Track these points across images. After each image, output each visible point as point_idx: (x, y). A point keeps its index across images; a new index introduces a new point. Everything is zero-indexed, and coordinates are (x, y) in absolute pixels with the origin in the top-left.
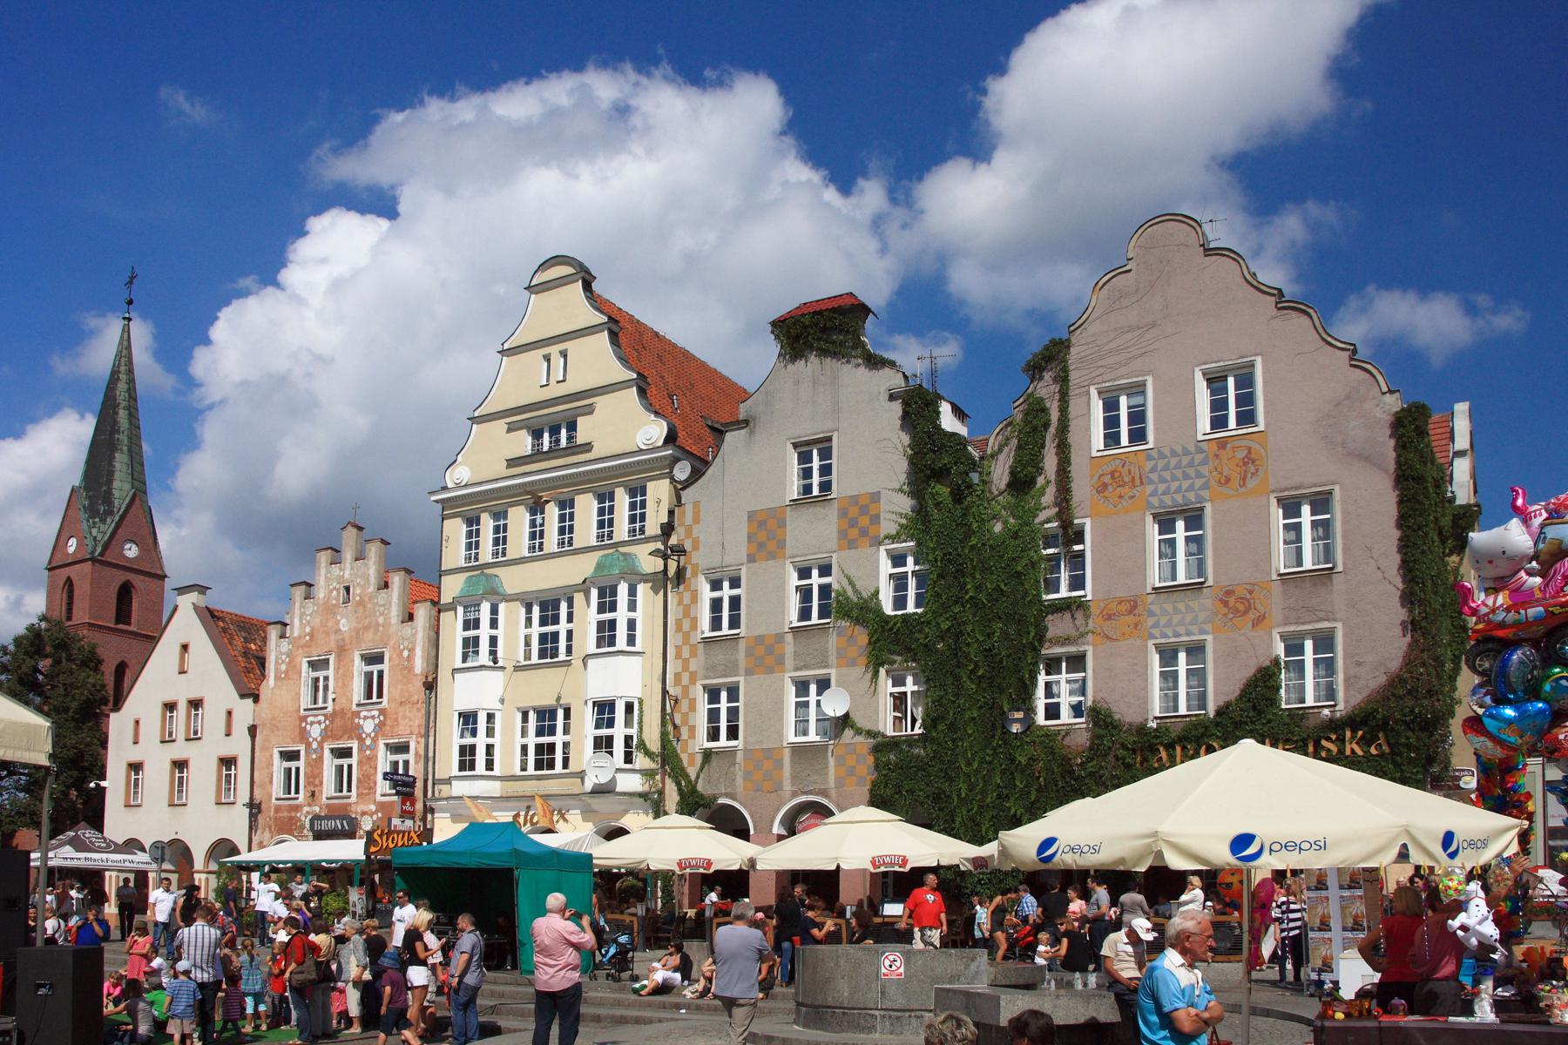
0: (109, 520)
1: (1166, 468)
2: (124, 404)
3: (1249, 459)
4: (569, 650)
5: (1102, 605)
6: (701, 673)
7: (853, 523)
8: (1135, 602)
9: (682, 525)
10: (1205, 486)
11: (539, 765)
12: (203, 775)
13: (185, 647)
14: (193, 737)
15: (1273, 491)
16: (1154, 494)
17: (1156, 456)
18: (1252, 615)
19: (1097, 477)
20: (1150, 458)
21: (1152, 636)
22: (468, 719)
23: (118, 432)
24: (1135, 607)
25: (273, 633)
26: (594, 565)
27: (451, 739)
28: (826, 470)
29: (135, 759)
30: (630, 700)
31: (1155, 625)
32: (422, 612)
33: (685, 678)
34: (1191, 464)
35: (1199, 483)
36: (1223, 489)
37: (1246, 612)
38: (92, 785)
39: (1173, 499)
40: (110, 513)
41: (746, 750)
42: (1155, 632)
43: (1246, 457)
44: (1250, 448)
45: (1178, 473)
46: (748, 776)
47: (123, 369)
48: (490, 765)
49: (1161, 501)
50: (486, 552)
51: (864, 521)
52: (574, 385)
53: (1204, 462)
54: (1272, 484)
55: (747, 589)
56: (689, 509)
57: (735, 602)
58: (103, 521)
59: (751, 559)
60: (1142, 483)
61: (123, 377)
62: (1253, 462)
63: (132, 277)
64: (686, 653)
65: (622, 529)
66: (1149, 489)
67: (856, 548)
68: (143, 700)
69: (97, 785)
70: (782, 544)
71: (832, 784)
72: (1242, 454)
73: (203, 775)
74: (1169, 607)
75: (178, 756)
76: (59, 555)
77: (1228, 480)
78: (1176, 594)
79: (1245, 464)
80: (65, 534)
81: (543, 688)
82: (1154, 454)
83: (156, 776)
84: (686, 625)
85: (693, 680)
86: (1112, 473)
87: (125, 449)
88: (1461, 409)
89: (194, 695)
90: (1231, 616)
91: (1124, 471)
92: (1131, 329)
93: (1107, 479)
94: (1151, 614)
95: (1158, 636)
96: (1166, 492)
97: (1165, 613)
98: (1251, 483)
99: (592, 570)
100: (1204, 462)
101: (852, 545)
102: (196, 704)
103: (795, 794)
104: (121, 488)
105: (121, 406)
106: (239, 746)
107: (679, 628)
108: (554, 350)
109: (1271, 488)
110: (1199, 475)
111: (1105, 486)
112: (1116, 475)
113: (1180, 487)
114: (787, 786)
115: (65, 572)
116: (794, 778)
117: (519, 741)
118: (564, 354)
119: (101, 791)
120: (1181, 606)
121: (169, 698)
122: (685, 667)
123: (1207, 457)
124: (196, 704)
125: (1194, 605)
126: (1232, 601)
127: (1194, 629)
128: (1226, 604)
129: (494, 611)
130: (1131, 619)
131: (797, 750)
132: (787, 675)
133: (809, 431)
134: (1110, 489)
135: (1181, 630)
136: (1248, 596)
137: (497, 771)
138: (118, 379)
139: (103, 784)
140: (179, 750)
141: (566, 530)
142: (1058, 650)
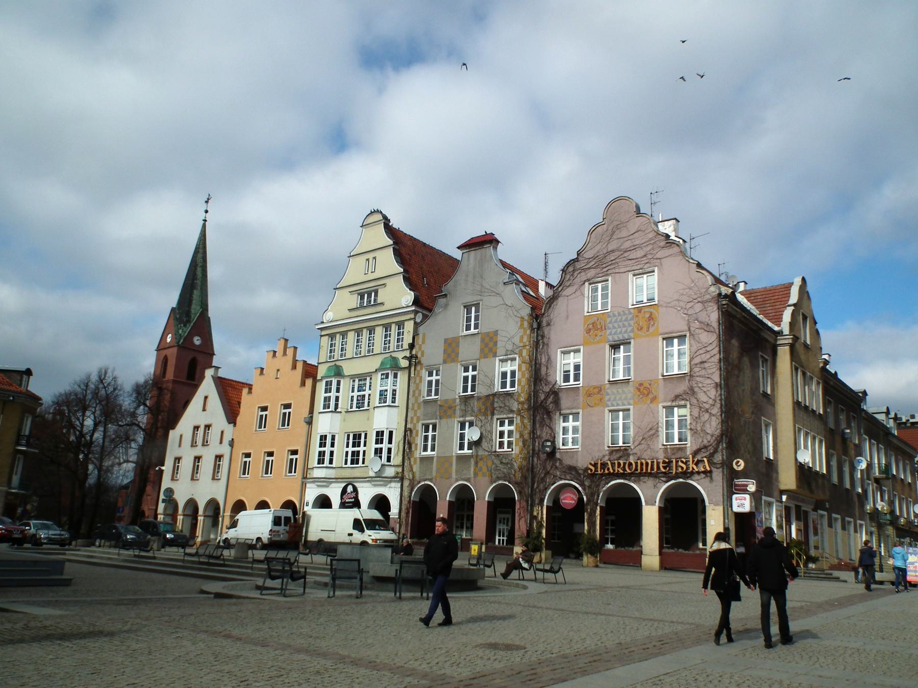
0: (188, 326)
1: (616, 322)
2: (200, 264)
3: (651, 318)
4: (369, 405)
5: (587, 389)
6: (422, 417)
7: (486, 345)
8: (601, 388)
9: (418, 344)
10: (632, 331)
11: (352, 463)
12: (207, 466)
13: (206, 398)
14: (205, 443)
15: (661, 334)
16: (611, 334)
17: (612, 315)
18: (651, 396)
19: (586, 326)
20: (609, 316)
21: (608, 406)
22: (323, 438)
23: (196, 279)
24: (600, 390)
25: (245, 391)
26: (380, 363)
27: (315, 449)
28: (477, 318)
29: (178, 455)
30: (391, 430)
31: (609, 400)
32: (309, 382)
33: (415, 421)
34: (626, 320)
35: (629, 329)
36: (639, 332)
37: (648, 395)
38: (157, 469)
39: (623, 336)
40: (189, 321)
41: (437, 457)
42: (609, 403)
43: (650, 317)
44: (651, 312)
45: (621, 324)
46: (438, 470)
47: (201, 246)
48: (331, 462)
49: (623, 336)
50: (337, 354)
51: (491, 345)
52: (377, 274)
53: (632, 319)
54: (661, 330)
55: (456, 376)
56: (421, 336)
57: (474, 377)
58: (185, 326)
59: (445, 362)
60: (605, 329)
61: (201, 251)
62: (653, 319)
63: (208, 199)
64: (416, 408)
65: (393, 345)
66: (608, 332)
67: (487, 358)
68: (184, 426)
69: (160, 468)
70: (457, 355)
71: (472, 476)
72: (647, 315)
73: (207, 466)
74: (615, 391)
75: (197, 454)
76: (162, 343)
77: (642, 328)
78: (623, 384)
79: (649, 320)
80: (167, 332)
81: (356, 423)
82: (611, 314)
83: (186, 465)
84: (417, 394)
85: (418, 422)
86: (593, 324)
87: (199, 288)
88: (37, 451)
89: (207, 423)
90: (641, 396)
91: (598, 323)
92: (495, 292)
93: (591, 326)
94: (608, 394)
95: (621, 404)
96: (615, 333)
97: (613, 394)
98: (651, 330)
99: (379, 365)
100: (632, 319)
101: (486, 357)
102: (208, 427)
103: (457, 480)
104: (195, 309)
105: (199, 265)
106: (225, 450)
107: (414, 395)
108: (370, 256)
109: (660, 332)
110: (630, 325)
111: (590, 330)
112: (595, 324)
113: (616, 331)
114: (454, 476)
115: (165, 352)
116: (457, 471)
117: (393, 446)
118: (375, 258)
119: (162, 472)
120: (620, 390)
121: (197, 424)
122: (415, 415)
123: (633, 316)
124: (208, 427)
125: (626, 390)
126: (642, 388)
127: (626, 402)
128: (639, 390)
129: (339, 383)
130: (598, 397)
131: (460, 458)
132: (456, 419)
133: (469, 299)
134: (592, 331)
135: (620, 403)
136: (649, 387)
137: (334, 465)
138: (198, 252)
139: (163, 468)
140: (199, 451)
141: (370, 344)
142: (568, 411)
